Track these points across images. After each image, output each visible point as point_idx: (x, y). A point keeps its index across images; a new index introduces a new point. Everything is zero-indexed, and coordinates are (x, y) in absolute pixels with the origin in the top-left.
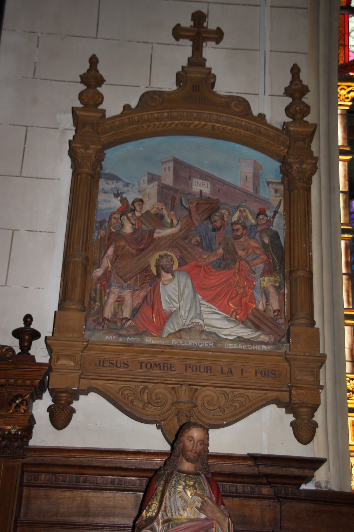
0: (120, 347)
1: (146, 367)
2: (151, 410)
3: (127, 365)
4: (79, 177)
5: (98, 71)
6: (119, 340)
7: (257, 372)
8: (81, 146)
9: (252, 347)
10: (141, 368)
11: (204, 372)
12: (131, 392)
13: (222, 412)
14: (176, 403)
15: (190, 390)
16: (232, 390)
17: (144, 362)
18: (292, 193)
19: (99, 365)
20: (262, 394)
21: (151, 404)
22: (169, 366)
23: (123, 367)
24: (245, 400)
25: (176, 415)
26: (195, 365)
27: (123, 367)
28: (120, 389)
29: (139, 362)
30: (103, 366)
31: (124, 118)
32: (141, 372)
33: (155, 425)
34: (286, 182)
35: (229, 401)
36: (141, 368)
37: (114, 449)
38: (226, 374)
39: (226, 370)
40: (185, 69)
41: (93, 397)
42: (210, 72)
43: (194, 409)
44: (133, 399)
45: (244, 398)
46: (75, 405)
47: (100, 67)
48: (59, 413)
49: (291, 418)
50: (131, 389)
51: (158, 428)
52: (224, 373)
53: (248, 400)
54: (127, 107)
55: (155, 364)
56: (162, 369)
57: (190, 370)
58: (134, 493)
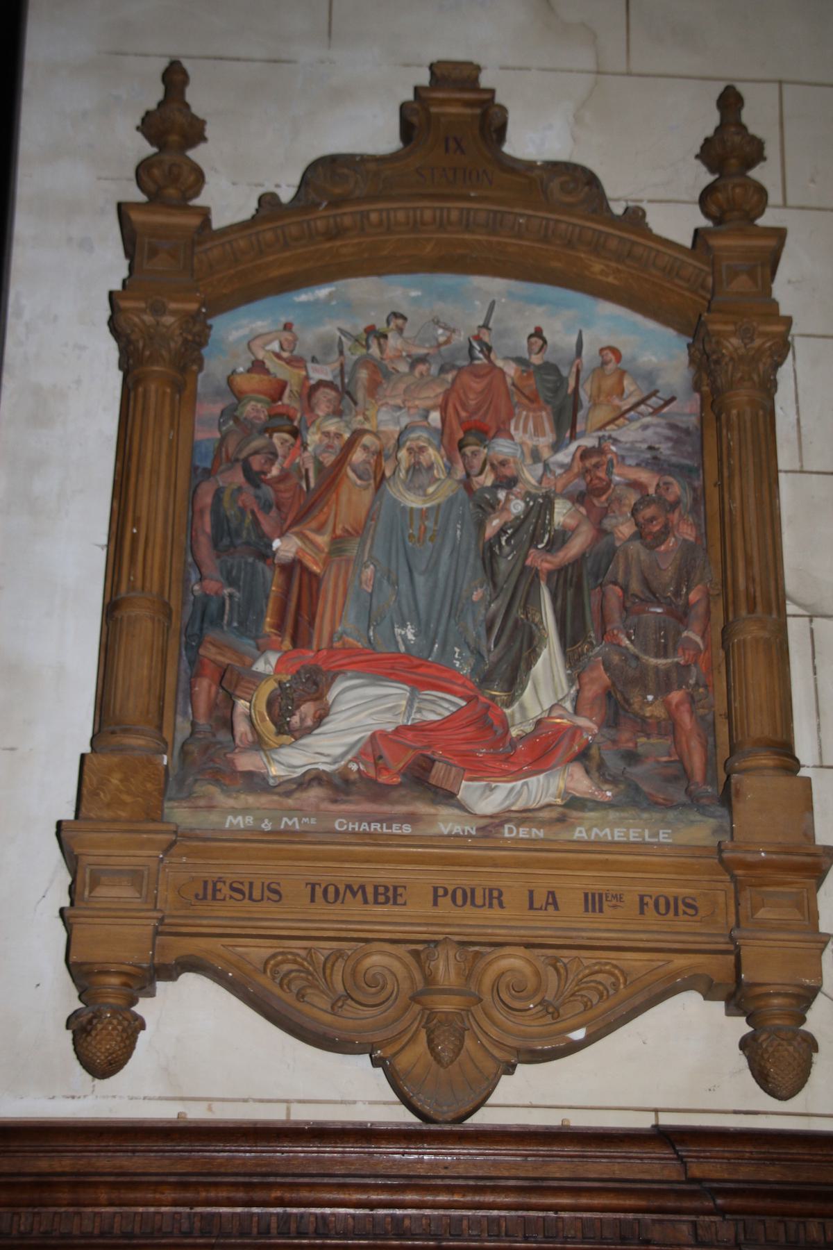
0: (367, 848)
1: (325, 892)
2: (356, 1017)
3: (276, 892)
4: (141, 389)
5: (187, 106)
6: (263, 826)
7: (218, 887)
8: (142, 305)
9: (348, 824)
10: (313, 900)
11: (484, 905)
12: (295, 967)
13: (550, 1016)
14: (423, 993)
15: (460, 957)
16: (574, 953)
17: (320, 884)
18: (723, 416)
19: (205, 897)
20: (661, 963)
21: (353, 999)
22: (390, 894)
23: (269, 899)
24: (613, 980)
25: (423, 1027)
26: (496, 889)
27: (269, 899)
28: (266, 963)
29: (307, 884)
30: (214, 898)
31: (259, 228)
32: (365, 912)
33: (368, 1055)
34: (705, 389)
35: (570, 981)
36: (313, 900)
37: (353, 1123)
38: (541, 909)
39: (540, 900)
40: (424, 94)
41: (192, 985)
42: (493, 98)
43: (472, 1008)
44: (304, 988)
45: (613, 974)
46: (143, 1008)
47: (746, 116)
48: (102, 1029)
49: (741, 1027)
50: (299, 959)
51: (376, 1063)
52: (536, 905)
53: (622, 980)
54: (268, 201)
55: (349, 887)
56: (370, 897)
57: (445, 901)
58: (486, 1244)
